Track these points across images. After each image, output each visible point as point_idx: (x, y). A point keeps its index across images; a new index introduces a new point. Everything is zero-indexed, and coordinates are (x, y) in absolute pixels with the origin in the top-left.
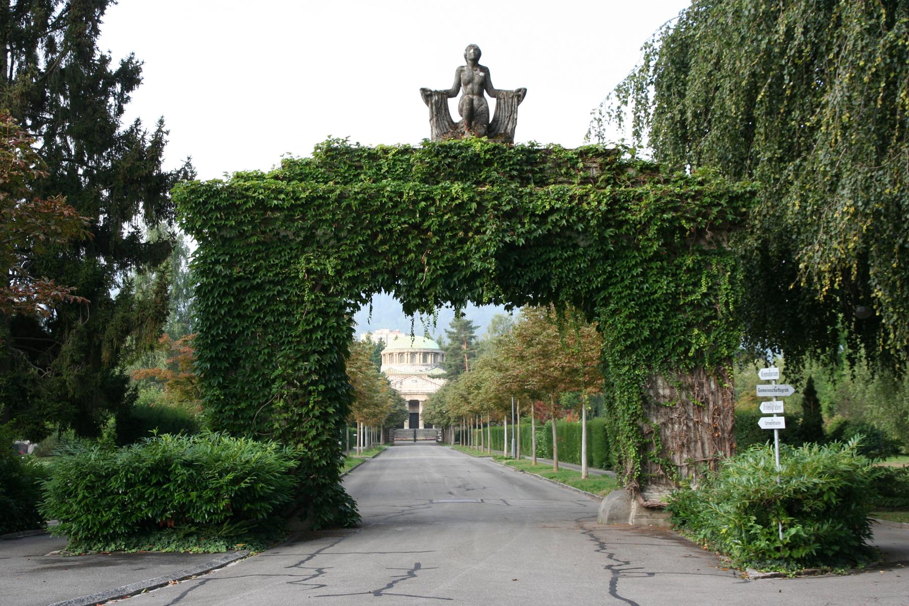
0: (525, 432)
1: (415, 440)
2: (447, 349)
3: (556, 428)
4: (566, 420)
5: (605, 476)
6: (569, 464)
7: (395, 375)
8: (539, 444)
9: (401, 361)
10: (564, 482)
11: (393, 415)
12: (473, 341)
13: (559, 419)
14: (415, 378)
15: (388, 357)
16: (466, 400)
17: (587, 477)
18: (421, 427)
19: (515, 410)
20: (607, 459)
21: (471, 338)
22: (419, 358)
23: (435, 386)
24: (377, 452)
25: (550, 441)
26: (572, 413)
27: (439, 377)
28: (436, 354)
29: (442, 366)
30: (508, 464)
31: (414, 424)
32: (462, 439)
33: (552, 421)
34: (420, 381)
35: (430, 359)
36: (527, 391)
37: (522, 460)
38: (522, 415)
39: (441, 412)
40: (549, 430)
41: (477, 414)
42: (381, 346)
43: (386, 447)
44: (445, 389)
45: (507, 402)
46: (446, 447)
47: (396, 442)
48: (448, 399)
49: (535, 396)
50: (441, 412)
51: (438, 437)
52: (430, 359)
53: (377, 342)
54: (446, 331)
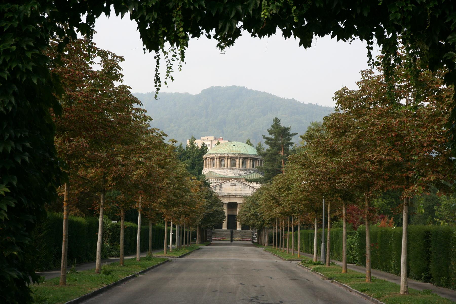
0: (336, 238)
1: (232, 241)
2: (264, 155)
3: (370, 234)
4: (380, 225)
5: (428, 291)
6: (383, 273)
7: (215, 178)
8: (351, 249)
9: (222, 165)
10: (379, 298)
11: (209, 215)
12: (290, 148)
13: (374, 223)
14: (234, 182)
15: (209, 161)
16: (277, 201)
17: (406, 292)
18: (239, 228)
19: (326, 211)
20: (427, 269)
21: (289, 144)
22: (238, 163)
23: (249, 190)
24: (187, 251)
25: (362, 246)
26: (386, 218)
27: (256, 181)
28: (255, 160)
29: (260, 170)
30: (316, 270)
31: (231, 225)
32: (275, 241)
33: (366, 226)
34: (239, 185)
35: (249, 164)
36: (339, 191)
37: (331, 266)
38: (334, 219)
39: (255, 215)
40: (362, 235)
41: (289, 215)
42: (204, 149)
43: (201, 246)
44: (260, 192)
45: (318, 204)
46: (260, 249)
47: (213, 242)
48: (260, 202)
49: (347, 197)
50: (255, 215)
51: (254, 239)
52: (249, 164)
53: (200, 147)
54: (264, 137)
